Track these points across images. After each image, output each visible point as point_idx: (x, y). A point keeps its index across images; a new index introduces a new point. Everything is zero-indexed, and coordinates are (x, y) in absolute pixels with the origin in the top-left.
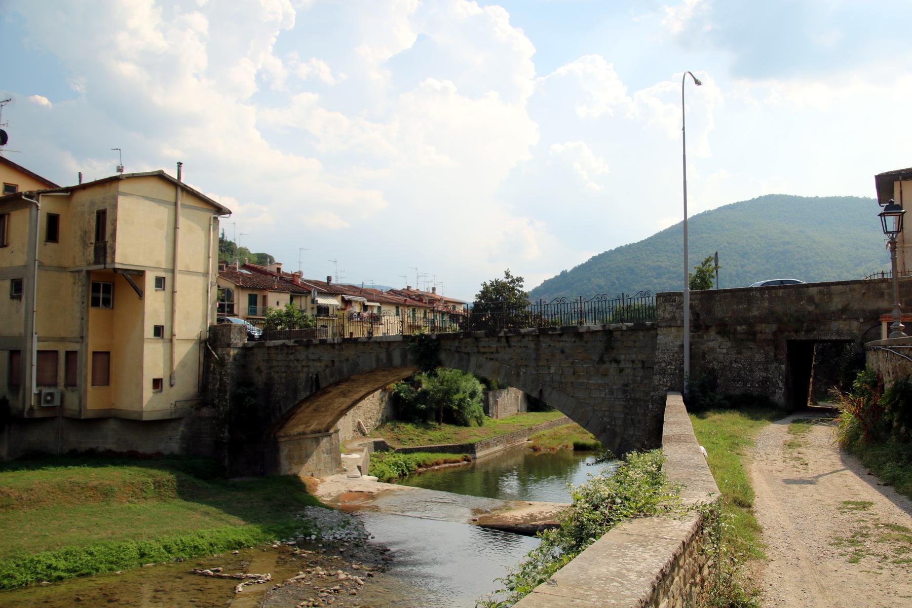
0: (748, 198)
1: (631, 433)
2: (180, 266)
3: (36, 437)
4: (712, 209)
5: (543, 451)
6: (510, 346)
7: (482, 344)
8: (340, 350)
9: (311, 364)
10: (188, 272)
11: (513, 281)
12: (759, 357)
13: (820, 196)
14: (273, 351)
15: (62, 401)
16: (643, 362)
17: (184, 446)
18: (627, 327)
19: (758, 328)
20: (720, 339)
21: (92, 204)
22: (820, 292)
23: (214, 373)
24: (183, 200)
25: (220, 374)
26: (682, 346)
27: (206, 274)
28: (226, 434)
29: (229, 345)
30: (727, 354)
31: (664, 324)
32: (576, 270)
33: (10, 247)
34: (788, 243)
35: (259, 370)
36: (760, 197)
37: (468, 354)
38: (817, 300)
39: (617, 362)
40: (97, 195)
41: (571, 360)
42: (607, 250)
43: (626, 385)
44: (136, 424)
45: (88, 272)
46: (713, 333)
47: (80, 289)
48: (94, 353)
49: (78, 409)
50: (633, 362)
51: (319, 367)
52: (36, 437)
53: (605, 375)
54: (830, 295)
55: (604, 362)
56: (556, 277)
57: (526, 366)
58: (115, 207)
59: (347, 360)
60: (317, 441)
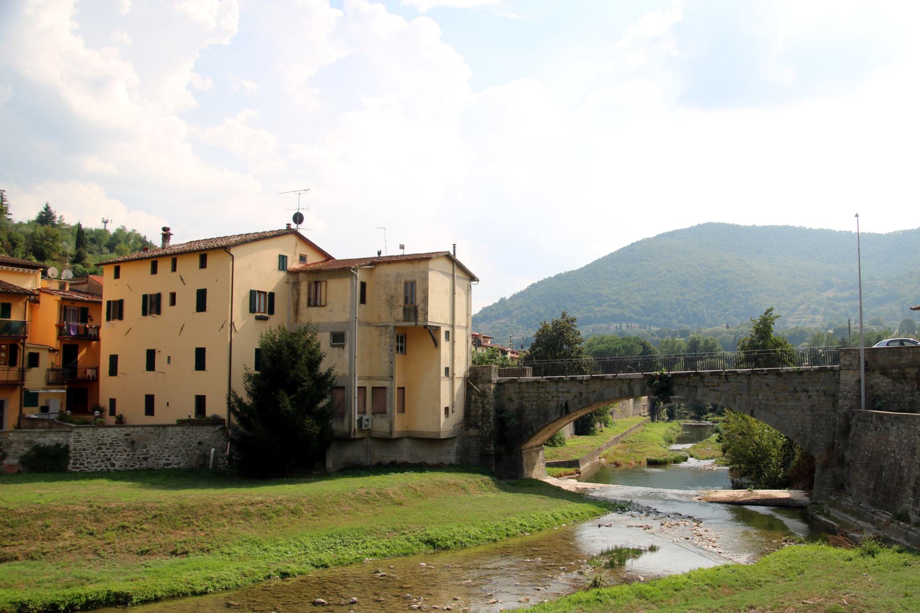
2: (456, 324)
3: (352, 453)
5: (624, 466)
7: (706, 380)
9: (560, 395)
10: (460, 327)
12: (907, 388)
13: (757, 225)
14: (524, 386)
19: (908, 370)
20: (882, 377)
21: (399, 276)
23: (476, 402)
24: (458, 273)
25: (482, 403)
26: (859, 381)
27: (467, 327)
28: (492, 448)
29: (490, 381)
32: (515, 297)
33: (329, 307)
34: (728, 272)
35: (510, 400)
37: (696, 387)
39: (807, 391)
40: (406, 271)
42: (546, 277)
43: (813, 406)
44: (433, 441)
46: (877, 374)
47: (388, 340)
49: (388, 431)
51: (569, 397)
52: (352, 453)
53: (798, 400)
55: (797, 392)
58: (426, 279)
59: (594, 392)
60: (538, 452)
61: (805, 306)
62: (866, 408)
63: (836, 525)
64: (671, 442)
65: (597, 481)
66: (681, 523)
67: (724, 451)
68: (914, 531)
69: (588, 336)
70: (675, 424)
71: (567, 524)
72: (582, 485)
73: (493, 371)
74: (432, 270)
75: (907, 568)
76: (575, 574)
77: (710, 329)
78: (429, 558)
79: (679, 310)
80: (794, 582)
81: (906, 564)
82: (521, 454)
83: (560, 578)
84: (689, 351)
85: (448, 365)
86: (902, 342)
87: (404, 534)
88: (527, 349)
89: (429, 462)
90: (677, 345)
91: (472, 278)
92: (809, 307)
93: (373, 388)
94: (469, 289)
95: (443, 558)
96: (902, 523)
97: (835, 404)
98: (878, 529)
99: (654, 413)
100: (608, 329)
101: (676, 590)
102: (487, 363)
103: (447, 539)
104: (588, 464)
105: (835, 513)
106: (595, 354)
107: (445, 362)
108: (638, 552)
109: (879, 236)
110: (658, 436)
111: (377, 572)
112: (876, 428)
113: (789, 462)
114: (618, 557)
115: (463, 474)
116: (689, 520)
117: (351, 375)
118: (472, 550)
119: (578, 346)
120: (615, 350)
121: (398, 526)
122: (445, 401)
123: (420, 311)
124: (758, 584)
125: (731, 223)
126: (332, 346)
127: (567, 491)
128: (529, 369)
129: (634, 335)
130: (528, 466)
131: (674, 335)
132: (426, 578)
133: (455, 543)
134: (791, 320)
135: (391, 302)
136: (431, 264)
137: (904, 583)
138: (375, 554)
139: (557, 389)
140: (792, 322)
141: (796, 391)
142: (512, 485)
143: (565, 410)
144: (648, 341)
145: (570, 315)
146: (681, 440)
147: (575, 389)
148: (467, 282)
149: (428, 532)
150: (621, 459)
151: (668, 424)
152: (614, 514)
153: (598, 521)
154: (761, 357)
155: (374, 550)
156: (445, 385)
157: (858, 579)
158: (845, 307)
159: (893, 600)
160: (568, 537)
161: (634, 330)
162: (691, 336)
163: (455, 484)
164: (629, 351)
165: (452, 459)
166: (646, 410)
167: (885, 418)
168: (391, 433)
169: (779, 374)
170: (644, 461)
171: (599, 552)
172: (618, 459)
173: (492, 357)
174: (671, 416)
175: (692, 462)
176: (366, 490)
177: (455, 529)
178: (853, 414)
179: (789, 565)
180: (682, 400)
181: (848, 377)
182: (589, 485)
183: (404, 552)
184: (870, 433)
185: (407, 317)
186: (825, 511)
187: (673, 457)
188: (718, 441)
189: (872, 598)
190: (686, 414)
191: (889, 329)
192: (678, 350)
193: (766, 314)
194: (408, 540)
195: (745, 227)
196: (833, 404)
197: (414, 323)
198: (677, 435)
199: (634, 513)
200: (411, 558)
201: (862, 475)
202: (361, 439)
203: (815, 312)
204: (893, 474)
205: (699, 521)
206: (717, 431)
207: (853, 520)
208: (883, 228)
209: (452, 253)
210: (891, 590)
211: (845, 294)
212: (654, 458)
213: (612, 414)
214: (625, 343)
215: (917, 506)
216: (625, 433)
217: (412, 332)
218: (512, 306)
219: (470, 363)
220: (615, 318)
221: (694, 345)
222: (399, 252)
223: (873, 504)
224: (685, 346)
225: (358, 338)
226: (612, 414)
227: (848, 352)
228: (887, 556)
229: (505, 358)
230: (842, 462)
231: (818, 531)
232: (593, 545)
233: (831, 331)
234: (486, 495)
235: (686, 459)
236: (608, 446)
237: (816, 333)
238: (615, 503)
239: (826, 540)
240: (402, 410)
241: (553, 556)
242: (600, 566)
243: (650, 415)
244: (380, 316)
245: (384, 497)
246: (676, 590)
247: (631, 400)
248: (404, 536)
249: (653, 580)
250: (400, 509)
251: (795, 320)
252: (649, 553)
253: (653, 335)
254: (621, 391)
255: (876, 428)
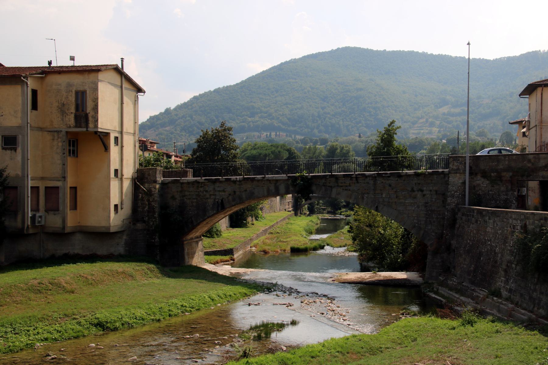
0: (328, 49)
1: (430, 228)
2: (125, 130)
3: (26, 247)
4: (297, 58)
5: (271, 253)
6: (358, 183)
8: (239, 185)
9: (217, 193)
11: (225, 130)
12: (503, 189)
13: (387, 50)
15: (45, 221)
16: (436, 191)
17: (127, 248)
18: (428, 172)
19: (504, 174)
20: (483, 180)
21: (69, 85)
22: (534, 157)
24: (126, 85)
25: (148, 201)
26: (464, 183)
27: (134, 134)
28: (157, 239)
29: (155, 182)
30: (486, 187)
31: (453, 172)
34: (361, 89)
35: (173, 198)
36: (338, 49)
37: (331, 187)
38: (532, 161)
39: (422, 191)
40: (77, 80)
41: (395, 190)
42: (207, 91)
43: (427, 203)
44: (104, 235)
45: (67, 132)
46: (479, 177)
47: (60, 144)
48: (71, 188)
50: (431, 191)
52: (26, 247)
53: (415, 198)
54: (539, 159)
56: (161, 113)
57: (368, 193)
58: (95, 89)
59: (246, 191)
60: (197, 243)
61: (425, 120)
62: (469, 205)
63: (444, 300)
64: (311, 233)
65: (248, 267)
66: (317, 300)
67: (354, 239)
68: (505, 305)
69: (242, 143)
70: (315, 218)
71: (222, 304)
72: (235, 270)
73: (158, 172)
74: (101, 81)
75: (498, 335)
76: (228, 347)
77: (345, 138)
78: (98, 340)
79: (319, 122)
80: (409, 348)
81: (497, 332)
82: (183, 244)
83: (215, 351)
84: (328, 156)
85: (117, 167)
86: (500, 151)
87: (74, 319)
88: (189, 153)
89: (99, 253)
90: (318, 151)
91: (139, 90)
92: (427, 121)
93: (46, 188)
94: (136, 100)
95: (112, 338)
96: (495, 298)
97: (444, 201)
98: (477, 303)
99: (297, 209)
100: (259, 137)
101: (312, 357)
102: (153, 165)
103: (115, 322)
104: (241, 252)
105: (443, 291)
106: (248, 158)
107: (114, 164)
108: (281, 326)
109: (487, 61)
110: (300, 227)
111: (49, 355)
112: (476, 221)
113: (407, 249)
114: (264, 331)
115: (130, 263)
116: (324, 298)
117: (24, 176)
118: (138, 330)
119: (233, 151)
120: (266, 155)
121: (69, 312)
122: (115, 199)
123: (90, 119)
124: (380, 350)
125: (365, 47)
126: (3, 148)
127: (222, 275)
128: (190, 171)
129: (281, 143)
130: (188, 254)
131: (315, 143)
132: (95, 358)
133: (123, 324)
134: (412, 131)
135: (62, 110)
136: (101, 76)
137: (495, 347)
138: (46, 339)
139: (214, 189)
140: (413, 133)
141: (413, 190)
142: (175, 271)
143: (220, 207)
144: (293, 148)
145: (228, 125)
146: (319, 231)
147: (229, 189)
148: (135, 93)
149: (98, 316)
150: (269, 247)
151: (309, 217)
152: (262, 294)
153: (247, 300)
154: (385, 162)
155: (46, 335)
156: (114, 185)
157: (460, 345)
158: (456, 121)
159: (486, 361)
160: (223, 317)
161: (282, 138)
162: (329, 143)
163: (123, 273)
164: (277, 155)
165: (121, 249)
166: (290, 206)
167: (484, 213)
168: (64, 228)
169: (399, 176)
170: (288, 249)
171: (248, 327)
172: (267, 248)
173: (157, 160)
174: (312, 211)
175: (328, 250)
176: (39, 281)
177: (123, 312)
178: (459, 210)
179: (405, 334)
180: (320, 198)
181: (455, 180)
182: (241, 270)
183: (75, 335)
184: (471, 225)
185: (78, 123)
186: (435, 289)
187: (312, 246)
188: (349, 231)
189: (470, 360)
190: (324, 209)
191: (492, 140)
192: (318, 156)
193: (389, 126)
194: (79, 323)
195: (377, 51)
196: (443, 201)
197: (85, 129)
198: (316, 227)
199: (279, 293)
200: (82, 340)
201: (465, 259)
202: (34, 234)
203: (432, 125)
204: (490, 259)
205: (332, 299)
206: (348, 224)
207: (457, 296)
208: (491, 56)
209: (120, 66)
210: (485, 353)
211: (457, 110)
212: (296, 246)
213: (261, 209)
214: (274, 149)
215: (507, 285)
216: (273, 226)
217: (83, 137)
218: (176, 115)
219: (137, 166)
220: (266, 128)
221: (332, 151)
222: (70, 63)
223: (473, 283)
224: (324, 152)
225: (31, 141)
226: (261, 209)
227: (456, 159)
228: (483, 325)
229: (169, 162)
230: (449, 249)
231: (428, 307)
232: (243, 321)
233: (444, 141)
234: (151, 281)
235: (322, 247)
236: (258, 236)
237: (433, 143)
238: (263, 285)
239: (435, 314)
240: (74, 207)
241: (209, 332)
242: (249, 338)
243: (293, 210)
244: (52, 122)
245: (57, 286)
246: (312, 357)
247: (278, 198)
248: (75, 321)
249: (291, 348)
250: (71, 297)
251: (416, 132)
252: (290, 327)
253: (297, 142)
254: (268, 190)
255: (476, 221)
